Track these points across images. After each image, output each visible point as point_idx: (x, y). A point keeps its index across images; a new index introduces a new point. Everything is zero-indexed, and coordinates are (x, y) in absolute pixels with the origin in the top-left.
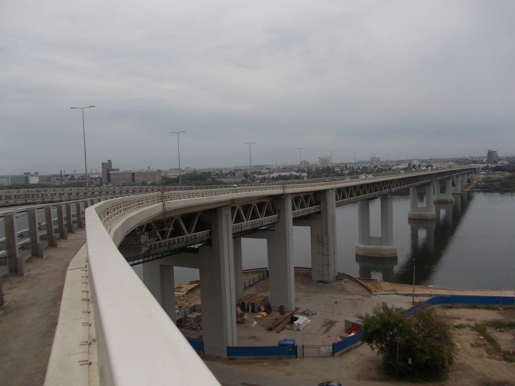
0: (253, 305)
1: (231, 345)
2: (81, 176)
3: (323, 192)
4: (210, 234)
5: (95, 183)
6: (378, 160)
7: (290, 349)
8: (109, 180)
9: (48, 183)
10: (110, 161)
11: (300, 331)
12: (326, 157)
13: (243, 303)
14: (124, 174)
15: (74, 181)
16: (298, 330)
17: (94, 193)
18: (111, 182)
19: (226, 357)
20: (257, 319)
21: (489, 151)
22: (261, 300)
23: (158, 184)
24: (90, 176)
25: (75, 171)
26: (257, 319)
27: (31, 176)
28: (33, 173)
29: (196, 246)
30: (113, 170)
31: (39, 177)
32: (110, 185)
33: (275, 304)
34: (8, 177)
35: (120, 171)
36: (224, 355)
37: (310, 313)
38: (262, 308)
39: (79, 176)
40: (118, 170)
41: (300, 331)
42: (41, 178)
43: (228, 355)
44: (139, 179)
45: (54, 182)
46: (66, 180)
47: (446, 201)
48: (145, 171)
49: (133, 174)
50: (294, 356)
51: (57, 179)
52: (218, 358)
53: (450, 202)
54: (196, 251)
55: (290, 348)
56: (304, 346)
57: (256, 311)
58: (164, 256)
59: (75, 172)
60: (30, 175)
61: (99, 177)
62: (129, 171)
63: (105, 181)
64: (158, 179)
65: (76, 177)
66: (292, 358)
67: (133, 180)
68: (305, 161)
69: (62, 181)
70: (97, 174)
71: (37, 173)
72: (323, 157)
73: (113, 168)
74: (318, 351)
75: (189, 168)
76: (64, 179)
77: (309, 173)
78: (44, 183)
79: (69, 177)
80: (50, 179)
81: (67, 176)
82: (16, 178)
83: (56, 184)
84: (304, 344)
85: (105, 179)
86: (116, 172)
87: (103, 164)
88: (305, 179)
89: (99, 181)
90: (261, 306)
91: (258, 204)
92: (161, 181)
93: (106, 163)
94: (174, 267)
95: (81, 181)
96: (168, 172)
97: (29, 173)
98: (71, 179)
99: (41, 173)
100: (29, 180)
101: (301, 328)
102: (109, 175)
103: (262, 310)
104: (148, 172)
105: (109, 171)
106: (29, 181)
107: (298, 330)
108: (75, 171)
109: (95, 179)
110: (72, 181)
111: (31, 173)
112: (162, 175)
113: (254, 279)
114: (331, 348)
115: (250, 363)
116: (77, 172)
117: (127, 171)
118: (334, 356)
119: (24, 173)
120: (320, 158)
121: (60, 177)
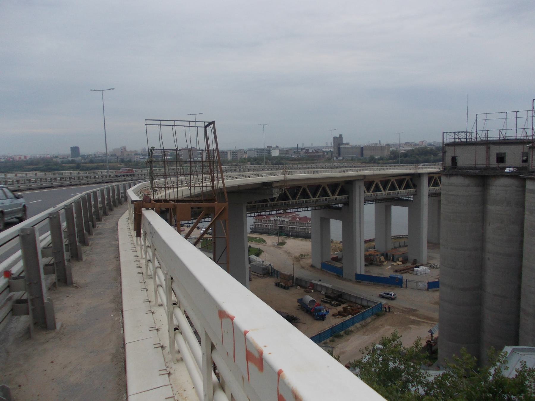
0: (393, 256)
1: (358, 273)
2: (314, 150)
3: (420, 175)
4: (348, 198)
5: (327, 156)
7: (397, 281)
8: (339, 154)
9: (286, 155)
10: (341, 136)
11: (418, 275)
13: (387, 254)
14: (354, 148)
15: (308, 154)
16: (416, 274)
17: (103, 176)
18: (341, 156)
19: (355, 280)
20: (392, 265)
22: (400, 254)
23: (386, 158)
24: (323, 149)
25: (312, 144)
26: (392, 265)
27: (272, 149)
28: (274, 146)
29: (340, 205)
30: (343, 144)
31: (279, 150)
32: (340, 159)
33: (411, 257)
34: (255, 150)
35: (350, 145)
36: (354, 278)
37: (435, 267)
38: (400, 259)
39: (313, 150)
40: (348, 144)
41: (418, 275)
42: (281, 151)
43: (356, 279)
44: (367, 154)
45: (292, 155)
46: (302, 153)
48: (373, 145)
49: (362, 148)
50: (400, 286)
51: (295, 152)
52: (350, 280)
54: (339, 208)
55: (397, 280)
56: (407, 281)
57: (395, 260)
58: (316, 210)
59: (312, 145)
60: (272, 148)
61: (330, 150)
62: (359, 145)
63: (335, 155)
64: (386, 153)
65: (310, 151)
66: (398, 287)
67: (362, 154)
69: (298, 153)
71: (277, 147)
73: (343, 142)
74: (417, 285)
75: (425, 141)
76: (300, 152)
77: (54, 178)
78: (283, 155)
79: (305, 150)
80: (288, 152)
81: (302, 149)
82: (261, 151)
83: (293, 157)
84: (407, 279)
85: (335, 153)
86: (347, 146)
87: (335, 138)
88: (158, 173)
89: (330, 154)
90: (400, 257)
91: (381, 182)
92: (389, 156)
94: (331, 220)
95: (314, 154)
96: (402, 145)
97: (271, 147)
98: (305, 152)
99: (281, 146)
100: (271, 152)
101: (419, 274)
102: (339, 149)
103: (400, 260)
104: (376, 146)
105: (339, 145)
106: (271, 154)
107: (416, 274)
108: (312, 144)
109: (327, 152)
110: (306, 154)
111: (273, 147)
112: (391, 149)
113: (405, 242)
114: (426, 284)
115: (369, 285)
117: (357, 145)
118: (428, 291)
119: (267, 147)
121: (297, 150)
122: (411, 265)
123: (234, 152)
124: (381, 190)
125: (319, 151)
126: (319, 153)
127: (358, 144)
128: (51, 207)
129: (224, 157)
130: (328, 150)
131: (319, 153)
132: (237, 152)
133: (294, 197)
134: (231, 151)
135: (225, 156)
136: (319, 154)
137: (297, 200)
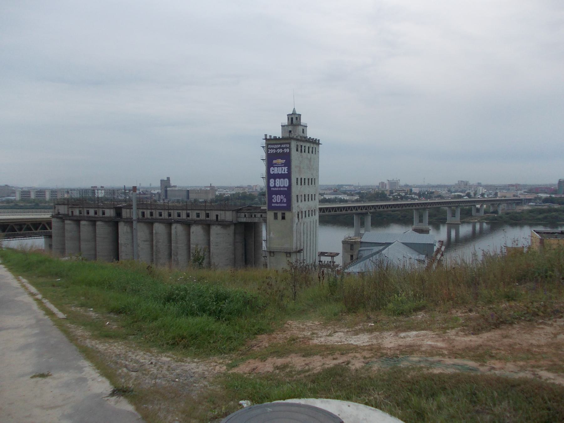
6: (466, 185)
10: (168, 179)
12: (395, 179)
21: (560, 180)
30: (170, 187)
40: (175, 186)
47: (422, 230)
53: (425, 231)
59: (150, 185)
61: (158, 193)
67: (188, 197)
68: (384, 183)
70: (284, 187)
71: (102, 187)
72: (392, 180)
85: (162, 195)
86: (173, 188)
87: (162, 181)
89: (157, 196)
93: (164, 180)
97: (96, 187)
102: (166, 191)
105: (166, 187)
116: (142, 185)
120: (388, 180)
122: (154, 264)
123: (54, 192)
124: (31, 229)
125: (147, 193)
126: (147, 194)
127: (189, 186)
128: (475, 225)
129: (41, 197)
130: (156, 192)
131: (147, 194)
132: (56, 192)
133: (36, 229)
134: (50, 191)
135: (43, 196)
136: (146, 196)
137: (38, 231)
